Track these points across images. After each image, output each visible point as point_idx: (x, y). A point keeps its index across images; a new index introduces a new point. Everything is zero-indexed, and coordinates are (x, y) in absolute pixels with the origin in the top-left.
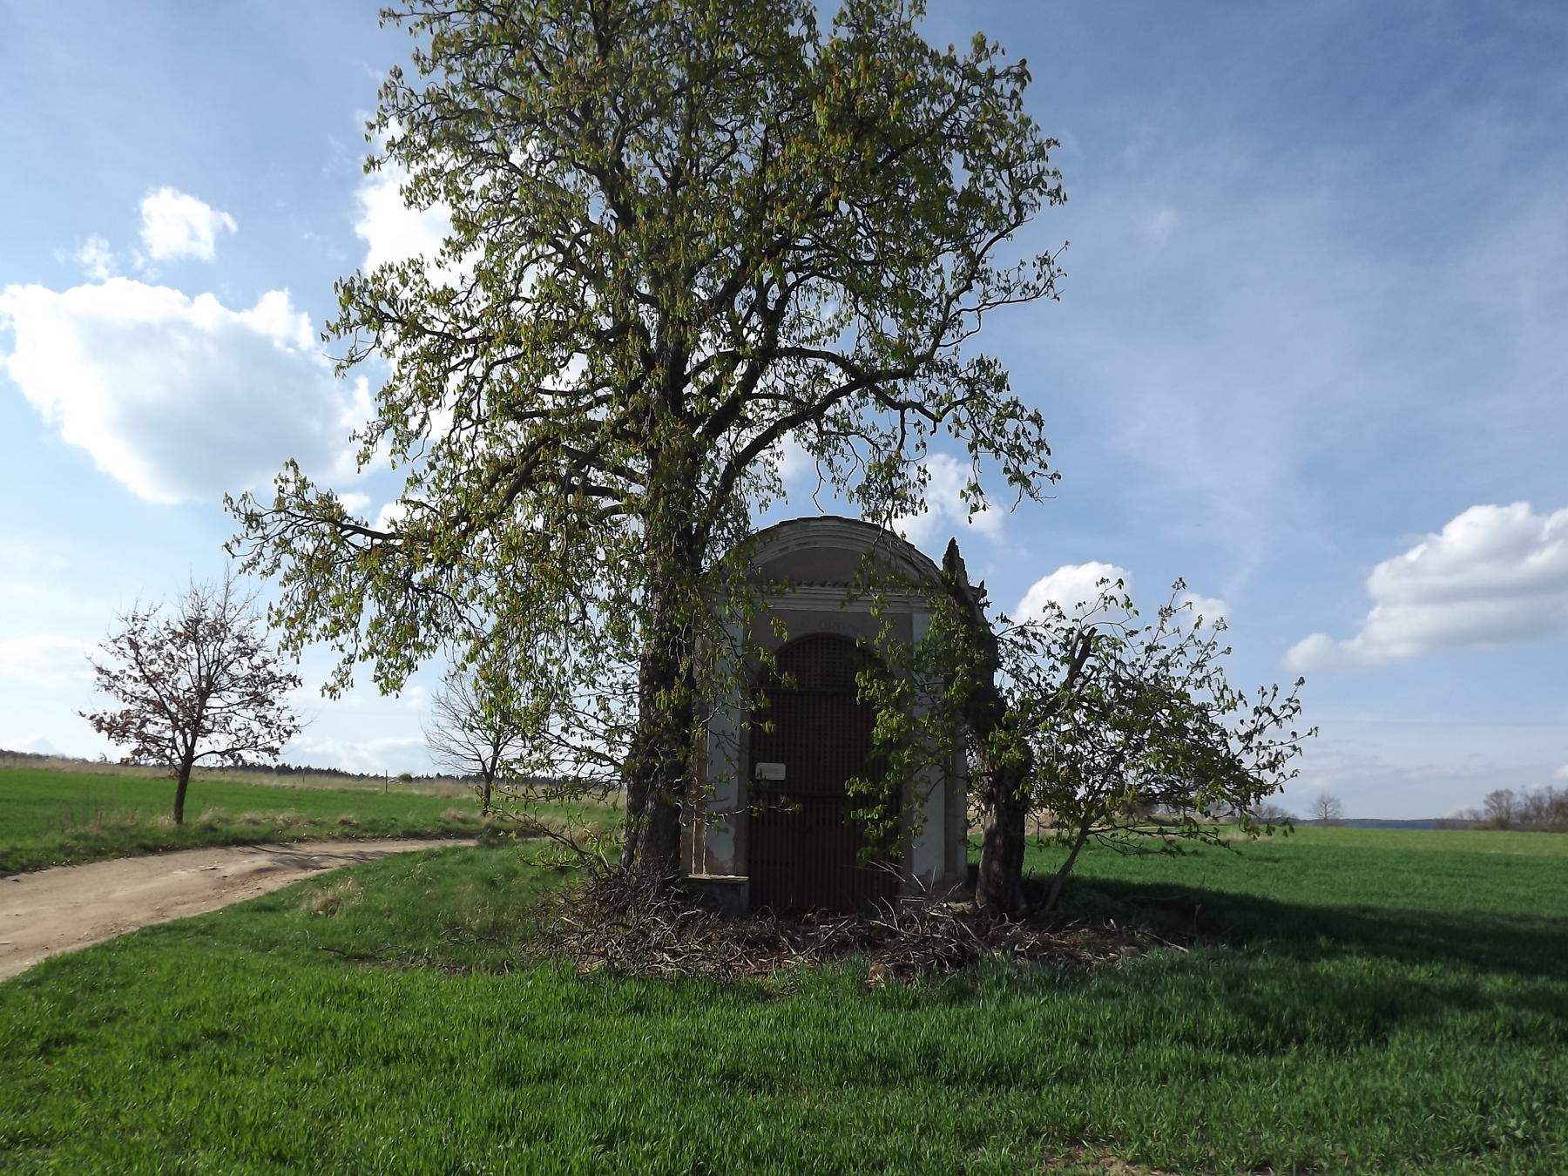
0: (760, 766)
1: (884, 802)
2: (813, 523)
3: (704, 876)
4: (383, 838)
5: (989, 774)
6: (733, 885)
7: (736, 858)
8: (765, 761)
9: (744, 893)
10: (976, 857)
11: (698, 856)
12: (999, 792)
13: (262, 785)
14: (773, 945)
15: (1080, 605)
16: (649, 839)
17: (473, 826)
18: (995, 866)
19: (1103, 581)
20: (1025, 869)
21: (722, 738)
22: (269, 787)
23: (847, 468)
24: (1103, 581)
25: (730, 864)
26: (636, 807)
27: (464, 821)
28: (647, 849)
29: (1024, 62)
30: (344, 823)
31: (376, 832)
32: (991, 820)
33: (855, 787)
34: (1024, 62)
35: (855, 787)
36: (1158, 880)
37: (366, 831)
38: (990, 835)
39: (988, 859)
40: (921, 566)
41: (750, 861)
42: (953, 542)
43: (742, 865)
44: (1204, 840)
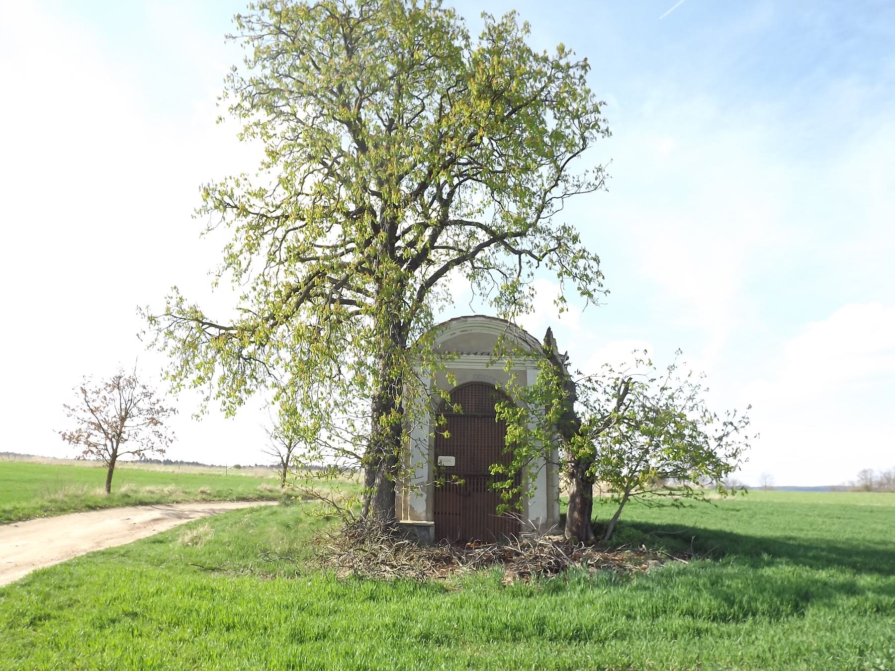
0: (440, 458)
2: (469, 319)
3: (409, 521)
6: (426, 527)
9: (432, 531)
10: (565, 510)
11: (406, 510)
12: (577, 472)
13: (155, 471)
14: (448, 561)
16: (377, 500)
18: (576, 515)
22: (159, 472)
25: (424, 515)
26: (370, 482)
27: (271, 491)
30: (203, 492)
32: (573, 488)
33: (496, 469)
35: (496, 469)
37: (215, 497)
38: (573, 497)
39: (572, 510)
40: (531, 343)
42: (549, 329)
43: (430, 515)
44: (696, 498)
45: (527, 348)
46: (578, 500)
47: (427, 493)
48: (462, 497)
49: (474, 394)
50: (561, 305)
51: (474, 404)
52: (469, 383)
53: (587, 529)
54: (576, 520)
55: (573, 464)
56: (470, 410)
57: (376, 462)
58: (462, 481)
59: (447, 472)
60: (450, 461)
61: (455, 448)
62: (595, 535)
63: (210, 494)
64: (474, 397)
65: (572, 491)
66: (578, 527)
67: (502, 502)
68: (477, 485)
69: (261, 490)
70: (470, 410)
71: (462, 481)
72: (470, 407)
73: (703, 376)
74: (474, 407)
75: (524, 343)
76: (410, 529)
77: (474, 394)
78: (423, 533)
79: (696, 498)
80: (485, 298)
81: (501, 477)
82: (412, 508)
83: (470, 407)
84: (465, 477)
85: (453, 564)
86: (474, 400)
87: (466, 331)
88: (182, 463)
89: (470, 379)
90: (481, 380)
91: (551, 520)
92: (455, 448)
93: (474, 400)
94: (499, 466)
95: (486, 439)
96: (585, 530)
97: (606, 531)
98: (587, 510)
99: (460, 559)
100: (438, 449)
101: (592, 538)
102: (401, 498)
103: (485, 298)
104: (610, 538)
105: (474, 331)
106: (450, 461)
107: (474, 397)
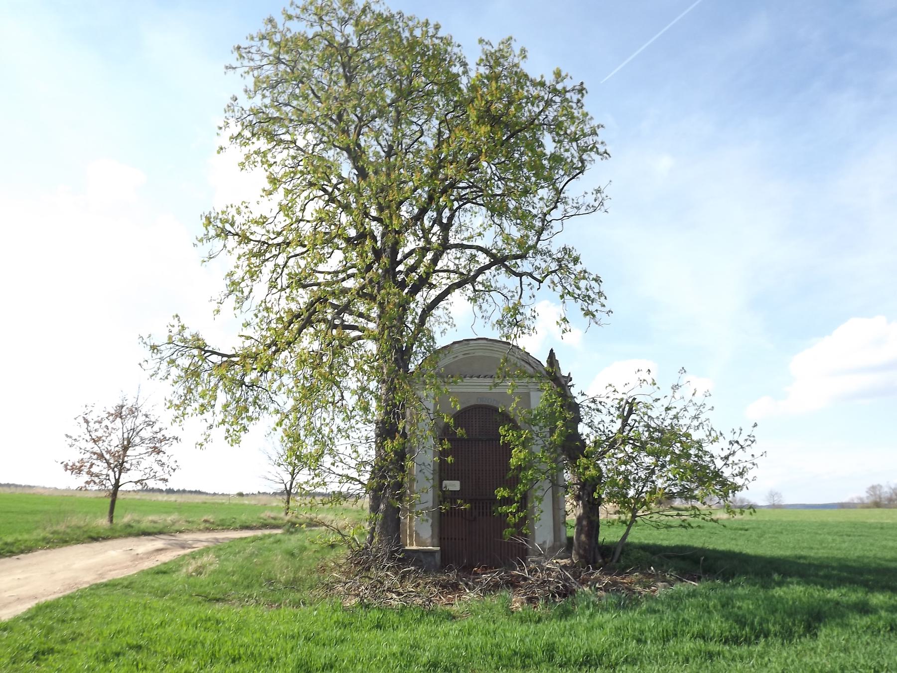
0: (445, 482)
1: (518, 502)
2: (471, 342)
3: (414, 547)
4: (228, 529)
6: (431, 553)
7: (432, 537)
9: (438, 557)
10: (572, 532)
11: (411, 536)
12: (583, 494)
18: (583, 537)
21: (423, 467)
22: (162, 501)
25: (429, 540)
26: (374, 508)
27: (274, 519)
30: (206, 521)
31: (224, 526)
32: (579, 511)
33: (501, 493)
35: (501, 493)
38: (580, 519)
39: (579, 533)
40: (534, 365)
41: (440, 539)
43: (436, 541)
46: (585, 523)
50: (563, 326)
54: (584, 542)
57: (380, 487)
58: (468, 506)
60: (454, 485)
62: (603, 558)
63: (213, 523)
65: (578, 514)
66: (585, 550)
71: (468, 506)
73: (708, 395)
81: (507, 501)
82: (417, 534)
84: (470, 501)
89: (473, 402)
90: (484, 403)
94: (505, 489)
97: (614, 554)
99: (467, 584)
101: (600, 561)
104: (618, 561)
105: (477, 354)
106: (454, 485)
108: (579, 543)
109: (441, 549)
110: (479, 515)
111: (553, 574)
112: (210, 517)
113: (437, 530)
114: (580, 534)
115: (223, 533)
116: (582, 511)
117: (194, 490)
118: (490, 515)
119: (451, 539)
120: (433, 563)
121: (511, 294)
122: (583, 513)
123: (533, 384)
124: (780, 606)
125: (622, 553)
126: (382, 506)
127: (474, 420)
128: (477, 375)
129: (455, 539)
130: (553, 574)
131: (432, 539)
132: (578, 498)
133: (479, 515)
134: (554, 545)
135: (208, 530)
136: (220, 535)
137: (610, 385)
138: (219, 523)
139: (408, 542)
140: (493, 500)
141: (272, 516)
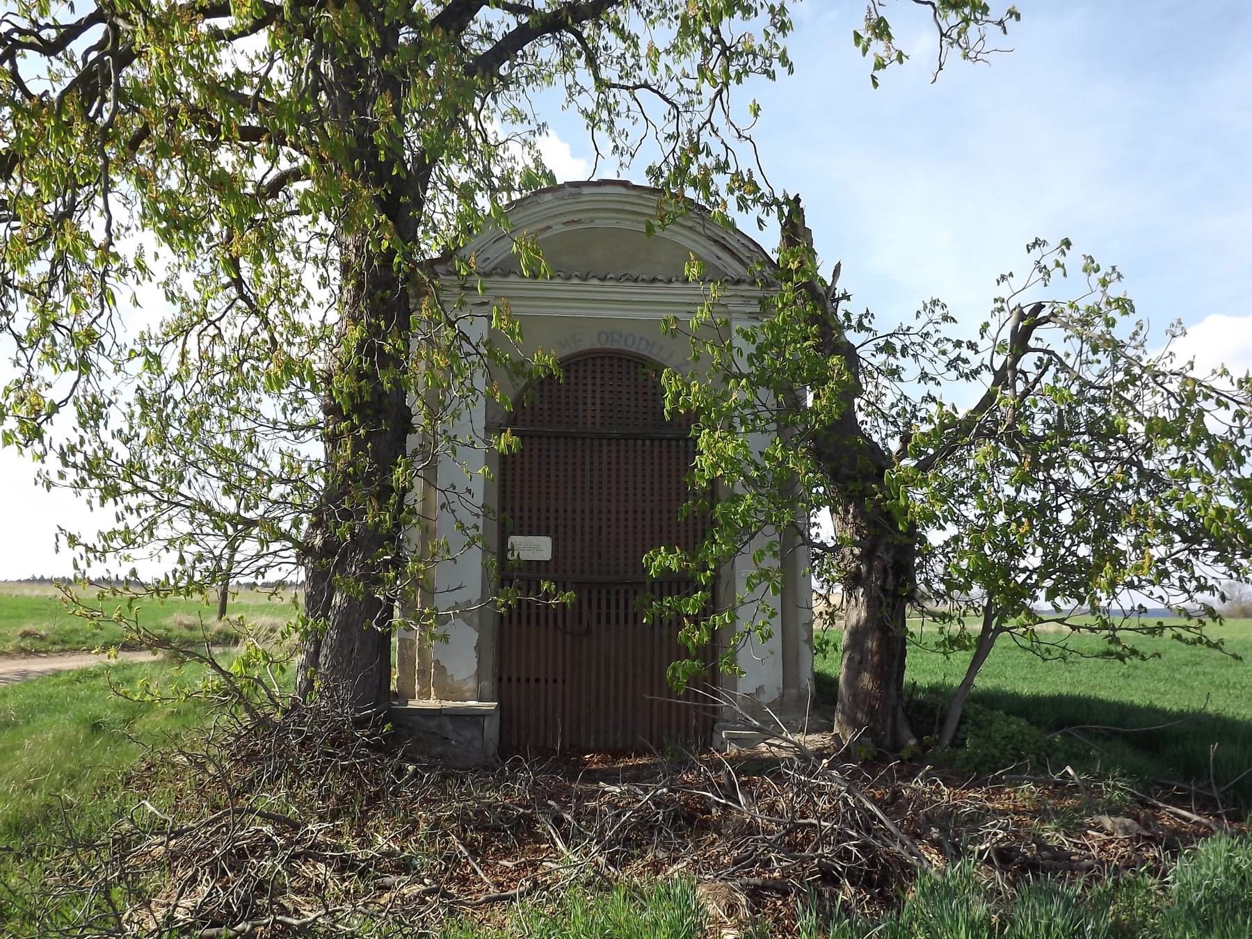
0: (514, 540)
1: (704, 588)
2: (586, 190)
3: (432, 703)
4: (75, 651)
5: (856, 544)
6: (473, 718)
7: (479, 676)
8: (521, 534)
9: (491, 729)
10: (835, 666)
11: (424, 673)
12: (869, 571)
13: (23, 596)
14: (525, 830)
15: (1003, 277)
16: (339, 649)
17: (200, 633)
18: (866, 680)
19: (1037, 243)
20: (908, 677)
21: (452, 497)
22: (30, 597)
23: (636, 132)
24: (1037, 243)
25: (471, 684)
26: (317, 601)
27: (191, 628)
28: (333, 668)
29: (754, 101)
30: (25, 635)
31: (66, 644)
32: (857, 614)
33: (663, 560)
34: (754, 101)
35: (663, 560)
36: (1064, 690)
37: (54, 643)
38: (857, 635)
39: (855, 669)
40: (744, 253)
41: (500, 680)
42: (864, 55)
43: (487, 685)
44: (1179, 637)
45: (735, 269)
46: (871, 644)
47: (480, 629)
48: (568, 638)
49: (598, 381)
50: (878, 47)
51: (598, 407)
52: (582, 354)
53: (894, 718)
54: (868, 693)
55: (857, 551)
56: (589, 421)
57: (329, 548)
58: (568, 597)
59: (533, 571)
60: (538, 548)
61: (552, 514)
62: (918, 735)
63: (42, 638)
64: (598, 389)
65: (853, 620)
66: (871, 713)
67: (683, 652)
68: (608, 607)
69: (170, 626)
70: (589, 421)
71: (568, 597)
72: (589, 414)
73: (1178, 331)
74: (598, 415)
75: (726, 257)
76: (432, 724)
77: (598, 381)
78: (468, 734)
79: (1179, 637)
80: (626, 158)
81: (678, 584)
82: (441, 669)
83: (589, 414)
84: (578, 586)
85: (539, 839)
86: (598, 394)
87: (579, 222)
88: (42, 580)
89: (588, 342)
90: (615, 346)
91: (793, 692)
92: (552, 514)
93: (598, 394)
94: (670, 550)
95: (631, 492)
96: (889, 720)
97: (942, 722)
98: (895, 669)
99: (558, 821)
100: (507, 515)
101: (912, 742)
102: (413, 643)
103: (626, 158)
104: (957, 743)
105: (598, 224)
106: (538, 548)
107: (598, 389)
108: (854, 695)
109: (500, 707)
110: (599, 621)
111: (823, 804)
112: (43, 628)
113: (490, 660)
114: (859, 673)
115: (38, 660)
116: (863, 614)
117: (29, 576)
118: (635, 621)
119: (528, 680)
120: (477, 744)
121: (684, 98)
122: (867, 620)
123: (740, 300)
124: (53, 463)
125: (962, 722)
126: (337, 599)
127: (589, 382)
128: (602, 275)
129: (537, 680)
130: (823, 804)
131: (479, 682)
132: (852, 581)
133: (599, 621)
134: (782, 696)
135: (25, 653)
136: (37, 665)
137: (935, 303)
138: (57, 638)
139: (417, 688)
140: (638, 583)
141: (186, 622)
